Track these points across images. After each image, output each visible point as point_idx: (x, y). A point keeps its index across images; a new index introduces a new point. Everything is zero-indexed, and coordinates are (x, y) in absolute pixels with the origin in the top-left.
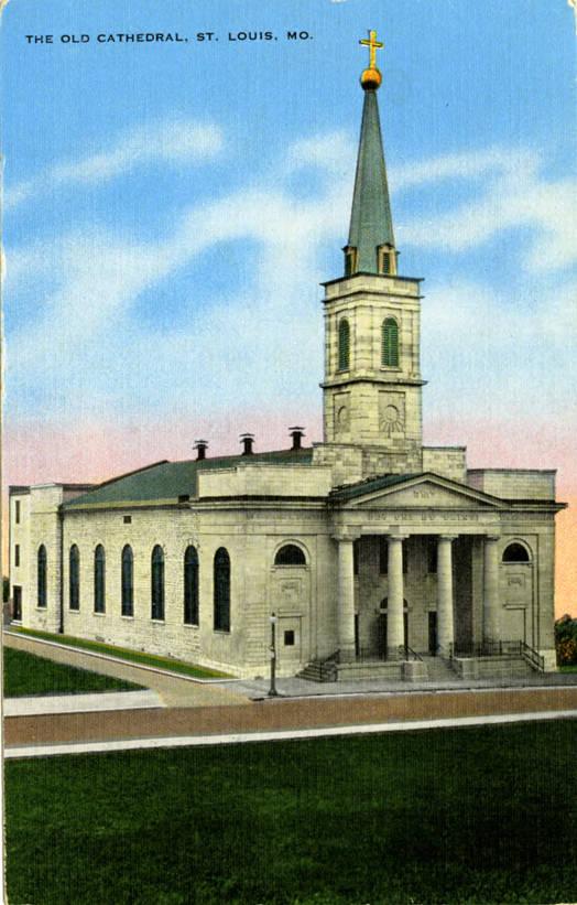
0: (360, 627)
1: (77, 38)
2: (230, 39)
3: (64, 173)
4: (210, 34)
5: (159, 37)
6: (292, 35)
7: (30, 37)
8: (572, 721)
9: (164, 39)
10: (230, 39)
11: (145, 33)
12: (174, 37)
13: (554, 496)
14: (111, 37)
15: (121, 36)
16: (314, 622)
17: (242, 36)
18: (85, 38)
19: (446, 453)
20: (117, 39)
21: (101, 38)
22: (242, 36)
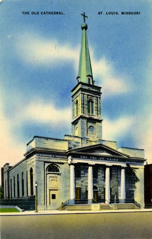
0: (26, 175)
1: (36, 13)
2: (107, 14)
3: (85, 167)
4: (101, 12)
5: (57, 13)
6: (123, 13)
7: (23, 12)
8: (1, 212)
9: (59, 13)
10: (107, 14)
11: (128, 14)
12: (61, 13)
13: (144, 157)
14: (45, 13)
15: (47, 12)
16: (63, 146)
17: (110, 13)
18: (38, 13)
19: (71, 204)
20: (46, 13)
21: (42, 13)
22: (110, 13)
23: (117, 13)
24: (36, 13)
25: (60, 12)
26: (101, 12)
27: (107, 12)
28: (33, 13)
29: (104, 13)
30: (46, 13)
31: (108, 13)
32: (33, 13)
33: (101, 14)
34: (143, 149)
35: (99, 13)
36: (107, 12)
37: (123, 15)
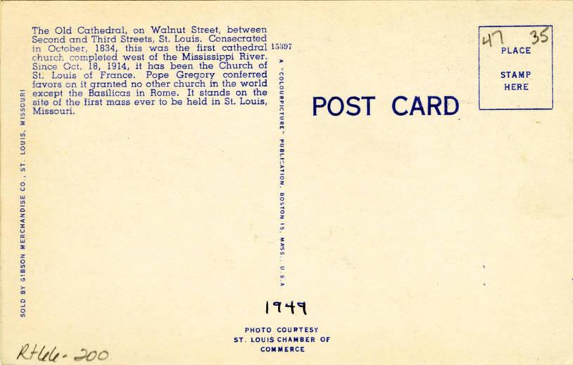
1: (23, 304)
2: (252, 341)
4: (241, 338)
6: (23, 123)
20: (282, 169)
23: (23, 256)
24: (23, 304)
25: (252, 58)
26: (241, 338)
27: (252, 339)
28: (164, 103)
29: (22, 159)
30: (282, 169)
31: (254, 340)
32: (323, 339)
33: (273, 45)
34: (347, 115)
35: (236, 340)
36: (252, 339)
37: (25, 123)
